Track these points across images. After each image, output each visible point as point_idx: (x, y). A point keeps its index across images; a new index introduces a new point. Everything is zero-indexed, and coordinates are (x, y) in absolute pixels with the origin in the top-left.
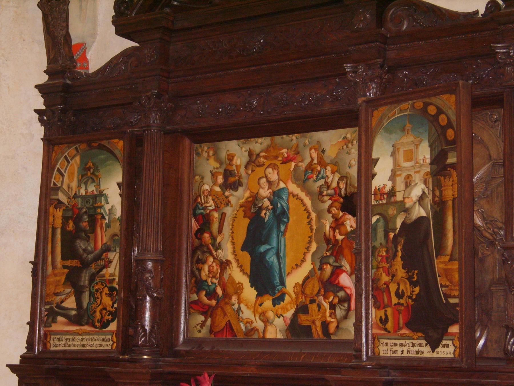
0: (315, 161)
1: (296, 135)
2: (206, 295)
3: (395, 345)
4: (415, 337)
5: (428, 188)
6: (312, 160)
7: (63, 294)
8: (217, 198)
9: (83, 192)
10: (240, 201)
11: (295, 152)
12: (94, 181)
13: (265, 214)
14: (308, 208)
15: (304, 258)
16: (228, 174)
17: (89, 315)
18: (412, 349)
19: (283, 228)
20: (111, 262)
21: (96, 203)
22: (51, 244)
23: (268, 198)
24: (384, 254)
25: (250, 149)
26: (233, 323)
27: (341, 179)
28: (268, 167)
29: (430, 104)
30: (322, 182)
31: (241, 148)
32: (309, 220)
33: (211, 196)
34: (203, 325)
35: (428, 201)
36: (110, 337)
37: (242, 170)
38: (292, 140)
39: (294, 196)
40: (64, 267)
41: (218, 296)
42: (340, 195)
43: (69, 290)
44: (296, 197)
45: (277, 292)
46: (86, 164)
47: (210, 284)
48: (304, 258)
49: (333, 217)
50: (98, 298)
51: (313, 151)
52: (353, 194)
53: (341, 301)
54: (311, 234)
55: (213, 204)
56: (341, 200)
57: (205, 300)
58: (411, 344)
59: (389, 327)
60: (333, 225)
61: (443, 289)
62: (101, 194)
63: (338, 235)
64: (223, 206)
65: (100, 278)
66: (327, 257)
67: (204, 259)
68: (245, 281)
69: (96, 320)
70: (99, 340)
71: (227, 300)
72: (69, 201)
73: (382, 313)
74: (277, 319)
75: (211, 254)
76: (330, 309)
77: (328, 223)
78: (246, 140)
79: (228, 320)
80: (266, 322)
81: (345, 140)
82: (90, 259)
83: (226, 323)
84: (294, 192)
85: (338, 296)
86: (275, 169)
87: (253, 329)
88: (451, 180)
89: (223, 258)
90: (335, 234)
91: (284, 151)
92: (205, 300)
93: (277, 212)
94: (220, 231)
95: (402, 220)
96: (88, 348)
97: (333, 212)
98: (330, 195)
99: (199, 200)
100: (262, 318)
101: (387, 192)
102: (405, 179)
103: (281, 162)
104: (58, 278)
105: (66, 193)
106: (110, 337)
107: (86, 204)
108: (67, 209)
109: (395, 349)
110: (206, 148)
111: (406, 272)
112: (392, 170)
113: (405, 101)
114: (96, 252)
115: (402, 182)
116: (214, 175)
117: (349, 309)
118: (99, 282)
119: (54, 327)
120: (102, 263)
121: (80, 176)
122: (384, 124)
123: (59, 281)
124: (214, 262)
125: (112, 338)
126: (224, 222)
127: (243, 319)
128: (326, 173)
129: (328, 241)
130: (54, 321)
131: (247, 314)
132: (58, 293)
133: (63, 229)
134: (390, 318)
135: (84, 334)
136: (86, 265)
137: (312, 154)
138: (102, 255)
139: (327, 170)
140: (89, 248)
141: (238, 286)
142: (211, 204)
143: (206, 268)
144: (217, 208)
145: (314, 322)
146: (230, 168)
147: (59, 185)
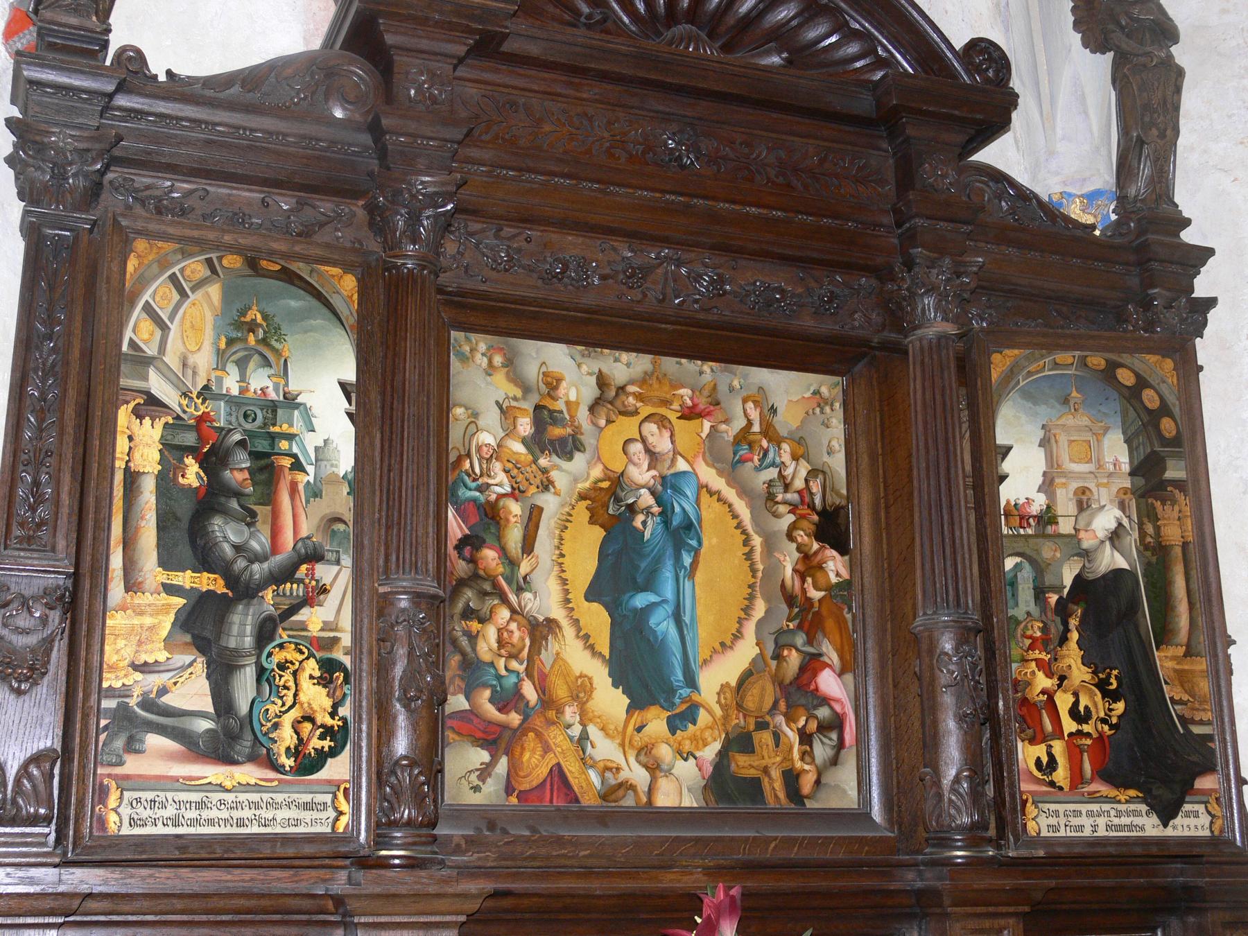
0: (756, 428)
1: (711, 363)
2: (491, 701)
3: (1077, 814)
4: (1122, 798)
5: (1129, 517)
6: (750, 423)
7: (170, 667)
8: (519, 468)
9: (231, 384)
10: (580, 486)
11: (710, 399)
12: (267, 363)
13: (644, 523)
14: (744, 524)
15: (739, 631)
16: (543, 416)
17: (259, 735)
18: (1116, 821)
19: (687, 560)
20: (324, 590)
21: (274, 425)
22: (121, 516)
23: (649, 489)
24: (1038, 634)
25: (600, 371)
26: (570, 772)
27: (813, 473)
28: (647, 419)
29: (1121, 365)
30: (772, 473)
31: (579, 366)
32: (747, 549)
33: (501, 461)
34: (485, 772)
35: (1132, 539)
36: (328, 798)
37: (583, 415)
38: (701, 373)
39: (711, 493)
40: (170, 589)
41: (528, 702)
42: (812, 507)
43: (188, 659)
44: (716, 497)
45: (677, 701)
46: (243, 313)
47: (503, 672)
48: (739, 631)
49: (799, 549)
50: (286, 688)
51: (750, 405)
52: (838, 509)
53: (823, 728)
54: (753, 580)
55: (506, 481)
56: (816, 518)
57: (491, 711)
58: (1113, 813)
59: (1061, 779)
60: (800, 567)
61: (1176, 707)
62: (290, 401)
63: (812, 588)
64: (533, 489)
65: (291, 633)
66: (789, 631)
67: (484, 610)
68: (600, 674)
69: (283, 750)
70: (293, 807)
71: (551, 714)
72: (185, 402)
73: (1040, 751)
74: (680, 763)
75: (505, 600)
76: (801, 743)
77: (788, 561)
78: (591, 349)
79: (554, 762)
80: (654, 768)
81: (818, 396)
82: (257, 576)
83: (551, 770)
84: (710, 486)
85: (817, 718)
86: (665, 427)
87: (620, 785)
88: (1176, 508)
89: (537, 613)
90: (806, 585)
91: (685, 392)
92: (491, 711)
93: (671, 523)
94: (528, 546)
95: (1076, 572)
96: (255, 829)
97: (799, 539)
98: (790, 504)
99: (467, 465)
100: (642, 758)
101: (1035, 513)
102: (1075, 493)
103: (679, 414)
104: (148, 621)
105: (176, 382)
106: (328, 798)
107: (241, 419)
108: (178, 424)
109: (1075, 821)
110: (482, 347)
111: (1093, 672)
112: (1045, 474)
113: (1066, 348)
114: (278, 558)
115: (1071, 500)
116: (506, 412)
117: (841, 745)
118: (290, 642)
119: (133, 765)
120: (297, 590)
121: (224, 340)
122: (1018, 382)
123: (152, 628)
124: (511, 619)
125: (333, 802)
126: (537, 527)
127: (595, 762)
128: (780, 457)
129: (790, 600)
130: (133, 746)
131: (604, 748)
132: (146, 663)
133: (166, 482)
134: (1061, 760)
135: (242, 788)
136: (243, 590)
137: (749, 411)
138: (296, 567)
139: (782, 451)
140: (254, 545)
141: (580, 681)
142: (500, 482)
143: (491, 632)
144: (517, 492)
145: (766, 770)
146: (548, 403)
147: (151, 350)
